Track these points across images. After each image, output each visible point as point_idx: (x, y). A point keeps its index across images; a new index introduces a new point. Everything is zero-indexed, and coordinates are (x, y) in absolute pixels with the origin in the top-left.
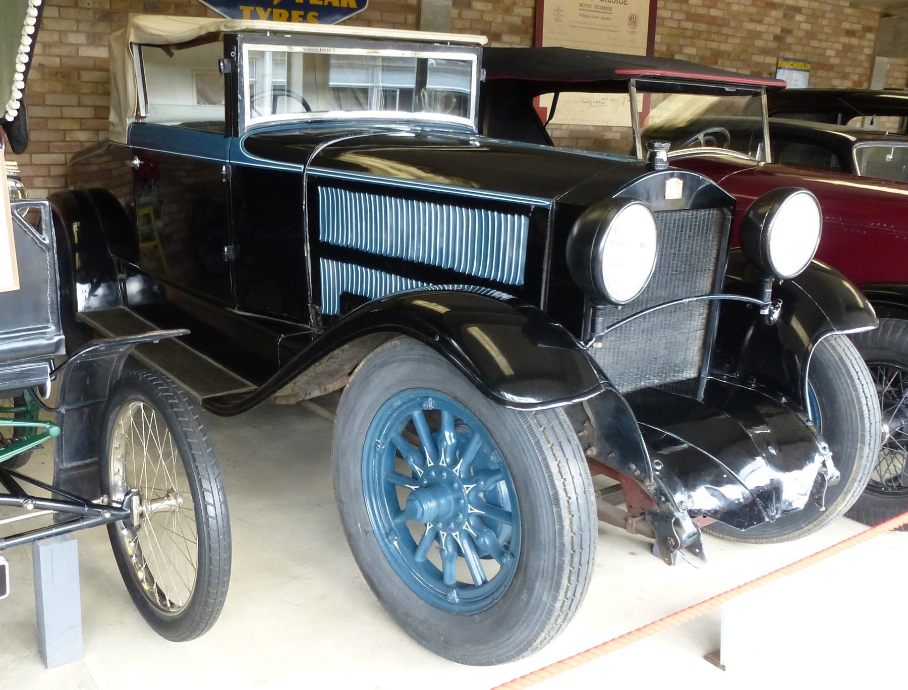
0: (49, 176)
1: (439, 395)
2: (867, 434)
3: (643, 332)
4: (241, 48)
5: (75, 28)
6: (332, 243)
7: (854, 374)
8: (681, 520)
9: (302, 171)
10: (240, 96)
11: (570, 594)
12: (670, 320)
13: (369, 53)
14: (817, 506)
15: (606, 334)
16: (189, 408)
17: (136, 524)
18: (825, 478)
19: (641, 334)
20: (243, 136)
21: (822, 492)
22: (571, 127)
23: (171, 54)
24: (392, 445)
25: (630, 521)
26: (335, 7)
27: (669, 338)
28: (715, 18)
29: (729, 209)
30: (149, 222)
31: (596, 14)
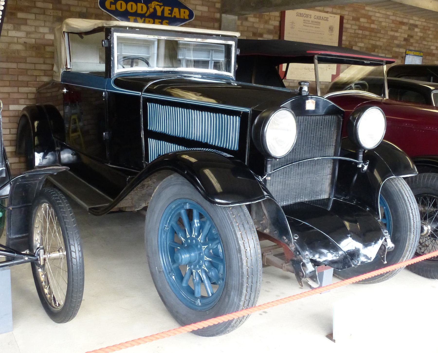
0: (27, 98)
1: (191, 202)
4: (113, 35)
5: (43, 25)
6: (153, 131)
7: (406, 198)
8: (306, 264)
9: (140, 95)
10: (112, 58)
11: (247, 298)
12: (312, 169)
14: (383, 261)
15: (272, 173)
16: (67, 205)
17: (42, 264)
18: (386, 247)
19: (297, 175)
20: (113, 77)
21: (384, 254)
23: (82, 37)
24: (172, 228)
25: (284, 265)
27: (312, 178)
28: (373, 29)
29: (341, 116)
30: (75, 123)
31: (312, 25)
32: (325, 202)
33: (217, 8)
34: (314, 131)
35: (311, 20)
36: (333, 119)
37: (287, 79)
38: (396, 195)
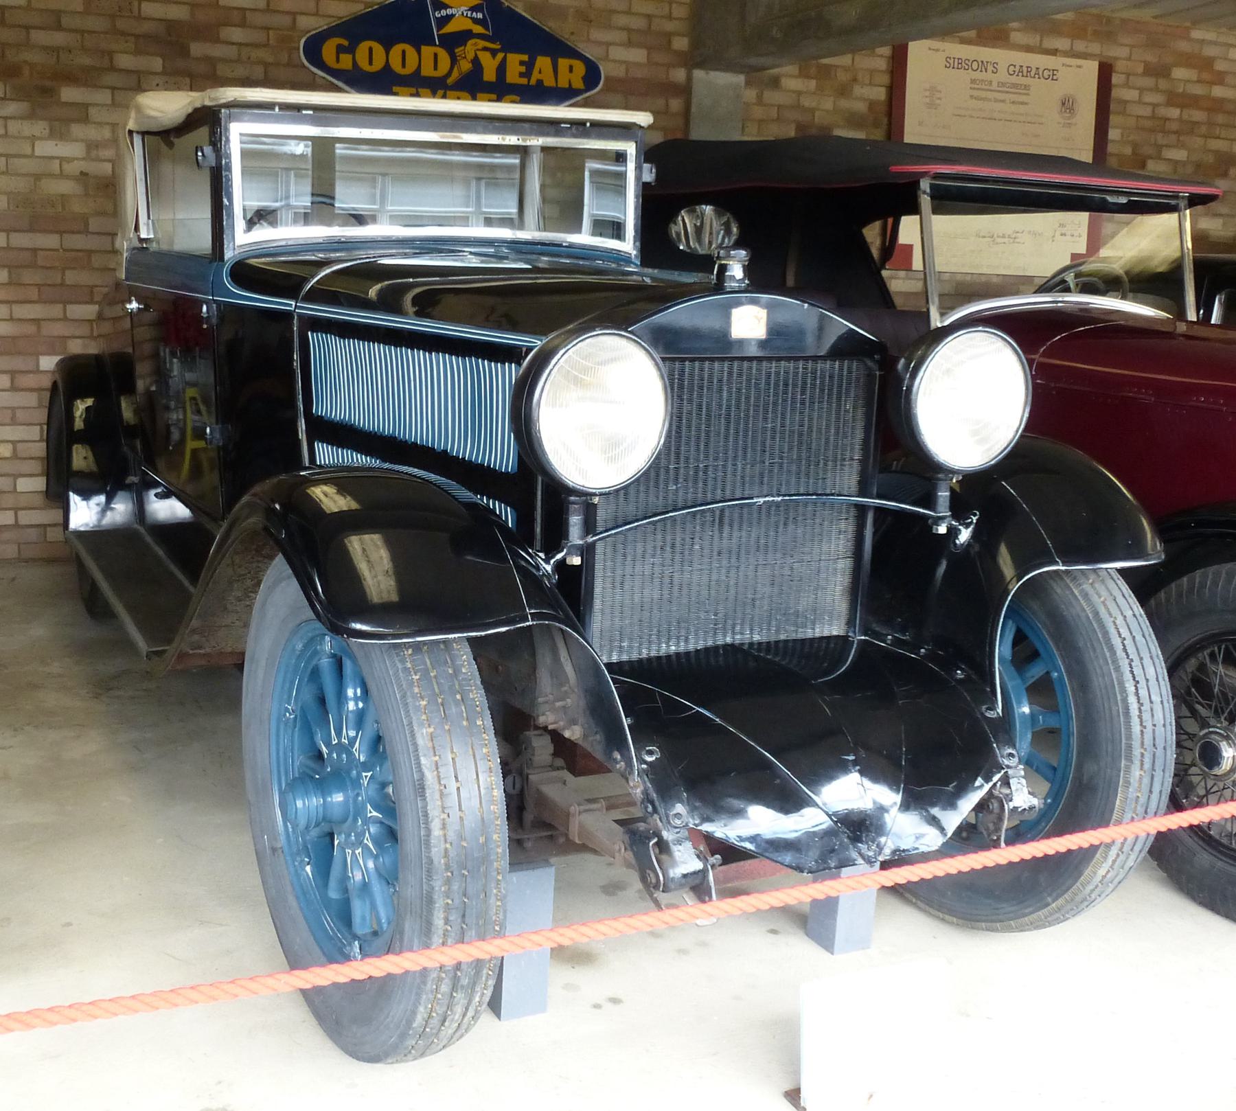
2: (1136, 744)
3: (719, 553)
4: (227, 130)
7: (1116, 642)
8: (671, 844)
9: (293, 309)
10: (225, 201)
13: (444, 137)
22: (959, 277)
23: (170, 145)
26: (548, 87)
28: (1222, 101)
32: (835, 646)
33: (679, 53)
34: (775, 411)
35: (995, 79)
36: (850, 372)
37: (914, 269)
38: (1084, 633)
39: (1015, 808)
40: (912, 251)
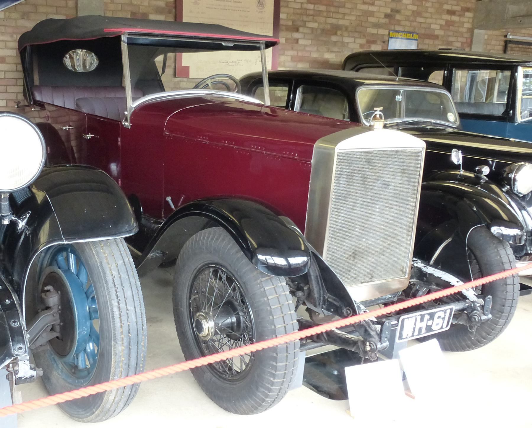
39: (20, 378)
40: (189, 69)
